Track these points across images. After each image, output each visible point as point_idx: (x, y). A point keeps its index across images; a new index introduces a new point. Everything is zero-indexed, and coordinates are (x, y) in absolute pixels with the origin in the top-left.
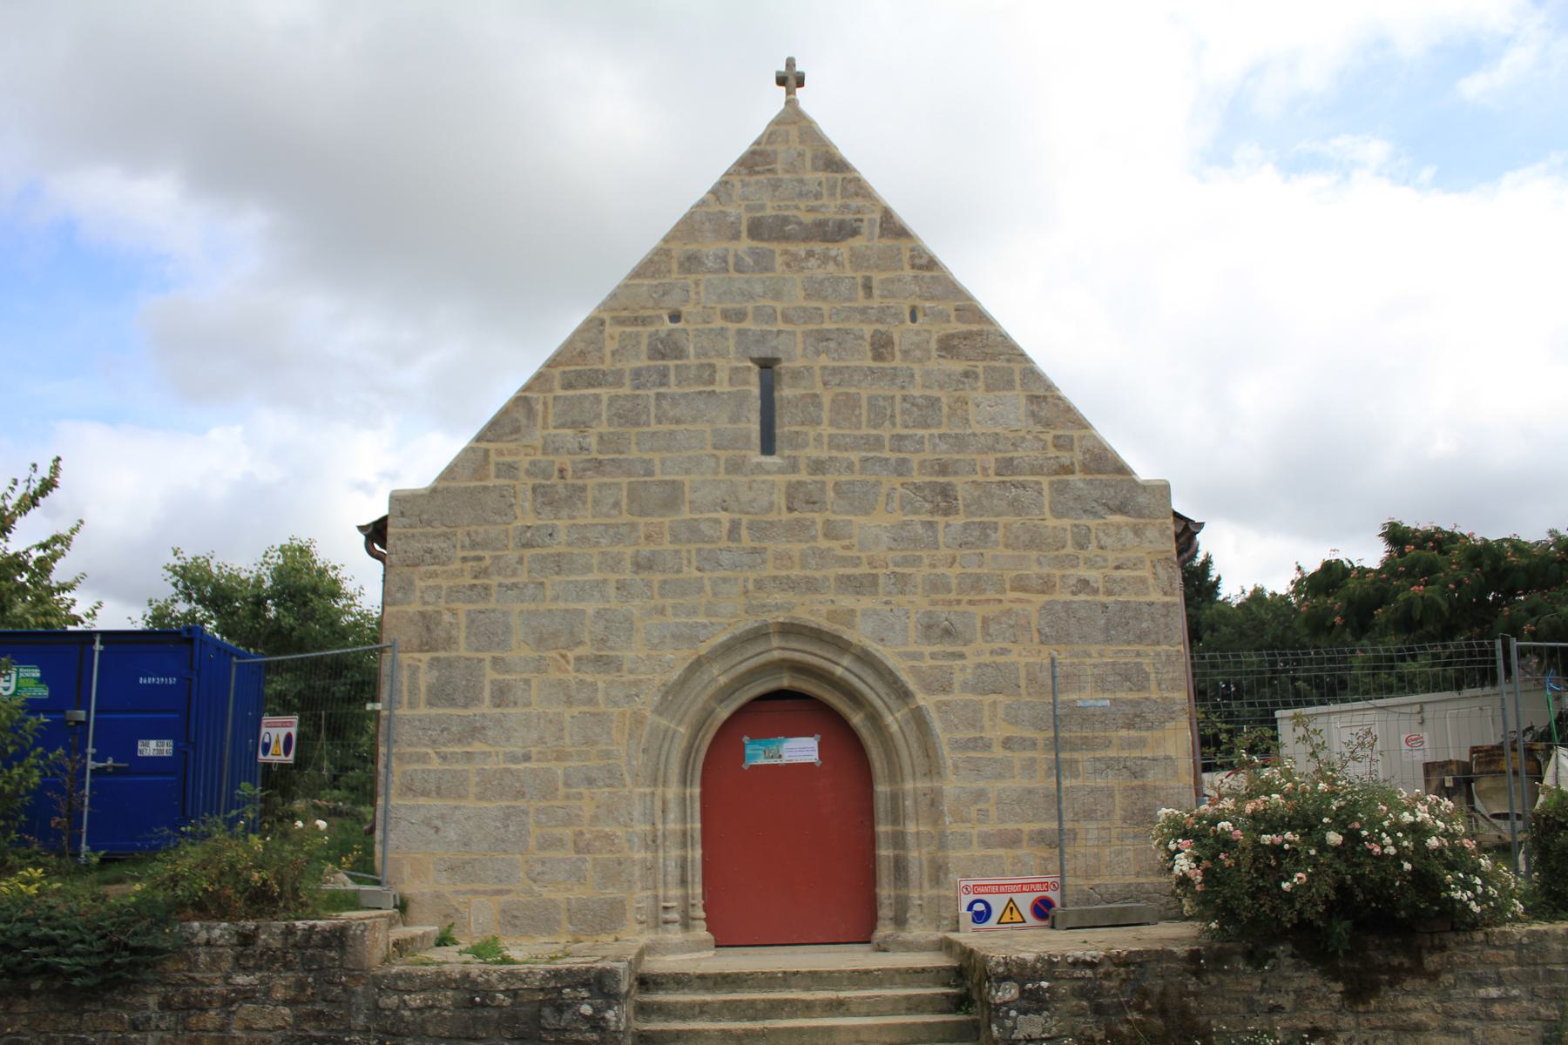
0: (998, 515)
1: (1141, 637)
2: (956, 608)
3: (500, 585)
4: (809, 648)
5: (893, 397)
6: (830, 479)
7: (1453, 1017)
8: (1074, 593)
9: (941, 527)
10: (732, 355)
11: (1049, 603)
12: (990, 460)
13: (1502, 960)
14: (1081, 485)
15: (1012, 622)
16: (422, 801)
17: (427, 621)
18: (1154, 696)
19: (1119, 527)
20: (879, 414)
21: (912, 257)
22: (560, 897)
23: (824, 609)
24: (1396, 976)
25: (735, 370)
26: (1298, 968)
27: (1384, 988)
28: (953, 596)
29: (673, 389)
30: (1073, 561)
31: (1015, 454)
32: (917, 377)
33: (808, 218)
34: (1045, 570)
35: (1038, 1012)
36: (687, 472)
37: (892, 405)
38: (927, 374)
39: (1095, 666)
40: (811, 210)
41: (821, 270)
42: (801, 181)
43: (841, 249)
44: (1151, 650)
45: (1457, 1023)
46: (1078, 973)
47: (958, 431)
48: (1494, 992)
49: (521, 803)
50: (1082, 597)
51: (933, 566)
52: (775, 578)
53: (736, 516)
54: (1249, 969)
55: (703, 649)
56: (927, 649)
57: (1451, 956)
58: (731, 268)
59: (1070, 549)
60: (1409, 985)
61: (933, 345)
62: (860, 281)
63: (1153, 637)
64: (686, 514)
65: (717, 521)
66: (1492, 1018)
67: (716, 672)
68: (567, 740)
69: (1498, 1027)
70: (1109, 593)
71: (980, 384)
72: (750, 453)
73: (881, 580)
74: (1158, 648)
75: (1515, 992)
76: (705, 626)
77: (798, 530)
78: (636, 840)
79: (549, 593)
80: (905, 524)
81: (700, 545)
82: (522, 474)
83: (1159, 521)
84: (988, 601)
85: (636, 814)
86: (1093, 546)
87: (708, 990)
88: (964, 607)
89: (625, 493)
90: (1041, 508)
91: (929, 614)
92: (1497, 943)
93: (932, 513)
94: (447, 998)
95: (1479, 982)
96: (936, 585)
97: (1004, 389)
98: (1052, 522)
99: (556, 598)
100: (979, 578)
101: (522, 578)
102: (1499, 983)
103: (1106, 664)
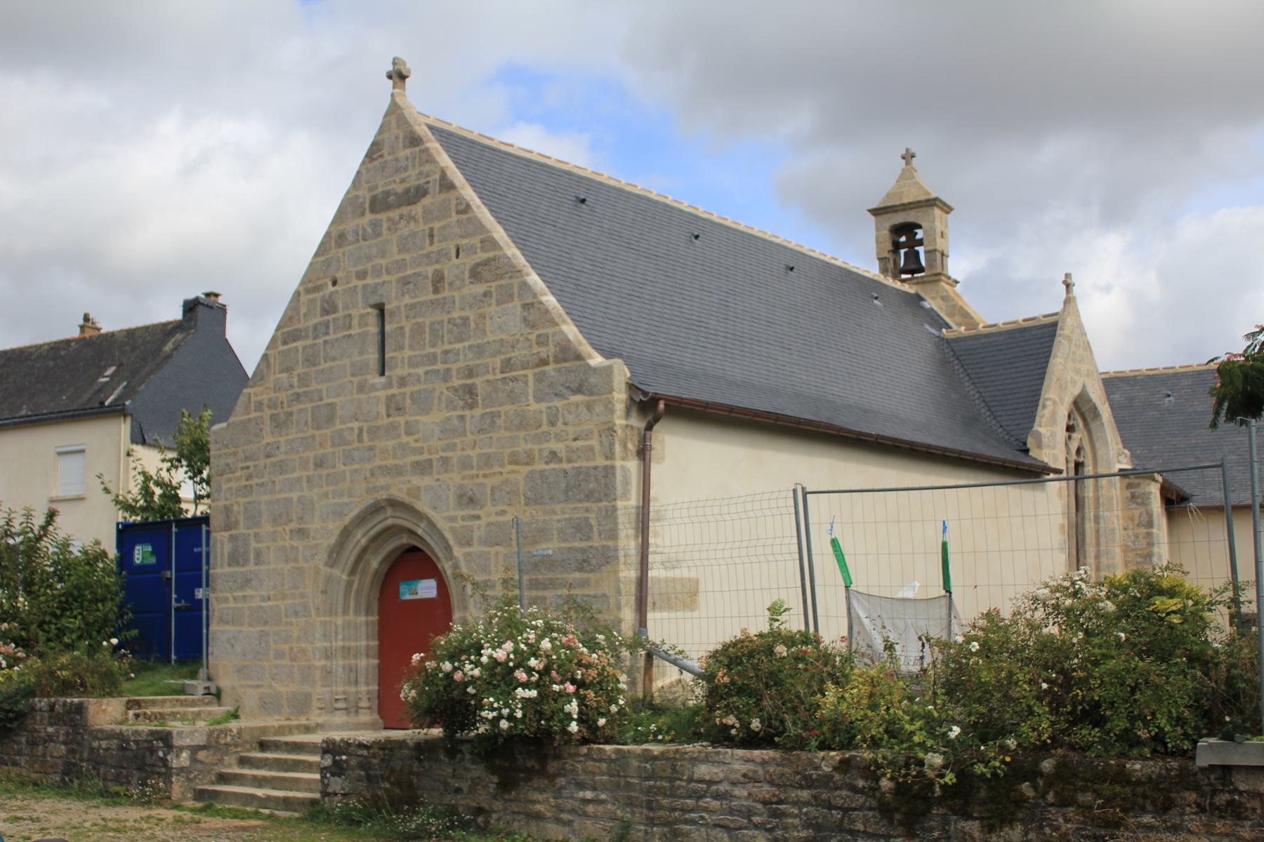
0: (501, 405)
1: (589, 496)
2: (476, 481)
3: (257, 485)
4: (375, 521)
5: (443, 321)
6: (408, 390)
7: (562, 811)
8: (547, 463)
9: (468, 419)
10: (360, 305)
11: (531, 472)
12: (497, 362)
13: (597, 770)
14: (553, 373)
15: (508, 489)
16: (227, 627)
17: (227, 510)
18: (596, 544)
19: (577, 406)
20: (436, 337)
21: (457, 205)
22: (283, 689)
23: (404, 487)
24: (530, 773)
25: (362, 316)
26: (474, 762)
27: (522, 783)
28: (474, 472)
29: (331, 337)
30: (545, 437)
31: (513, 355)
32: (457, 303)
33: (400, 188)
34: (530, 446)
35: (339, 776)
36: (339, 395)
37: (443, 328)
38: (463, 298)
39: (559, 521)
40: (402, 181)
41: (407, 229)
42: (397, 160)
43: (417, 209)
44: (594, 506)
45: (562, 816)
46: (360, 752)
47: (479, 341)
48: (589, 795)
49: (266, 628)
50: (552, 466)
51: (463, 449)
52: (380, 467)
53: (361, 424)
54: (447, 760)
55: (347, 520)
56: (460, 513)
57: (564, 764)
58: (360, 239)
59: (545, 428)
60: (536, 782)
61: (467, 275)
62: (427, 232)
63: (596, 495)
64: (338, 426)
65: (352, 429)
66: (585, 815)
67: (359, 535)
68: (286, 587)
69: (589, 822)
70: (569, 461)
71: (494, 301)
72: (369, 377)
73: (435, 464)
74: (600, 505)
75: (603, 796)
76: (347, 504)
77: (392, 429)
78: (317, 652)
79: (277, 487)
80: (448, 419)
81: (345, 447)
82: (265, 407)
83: (604, 397)
84: (494, 474)
85: (317, 635)
86: (560, 424)
87: (289, 752)
88: (481, 480)
89: (310, 414)
90: (527, 396)
91: (461, 486)
92: (595, 757)
93: (463, 408)
94: (114, 743)
95: (581, 786)
96: (465, 464)
97: (508, 302)
98: (534, 406)
99: (281, 491)
100: (489, 456)
101: (265, 479)
102: (594, 789)
103: (565, 519)
